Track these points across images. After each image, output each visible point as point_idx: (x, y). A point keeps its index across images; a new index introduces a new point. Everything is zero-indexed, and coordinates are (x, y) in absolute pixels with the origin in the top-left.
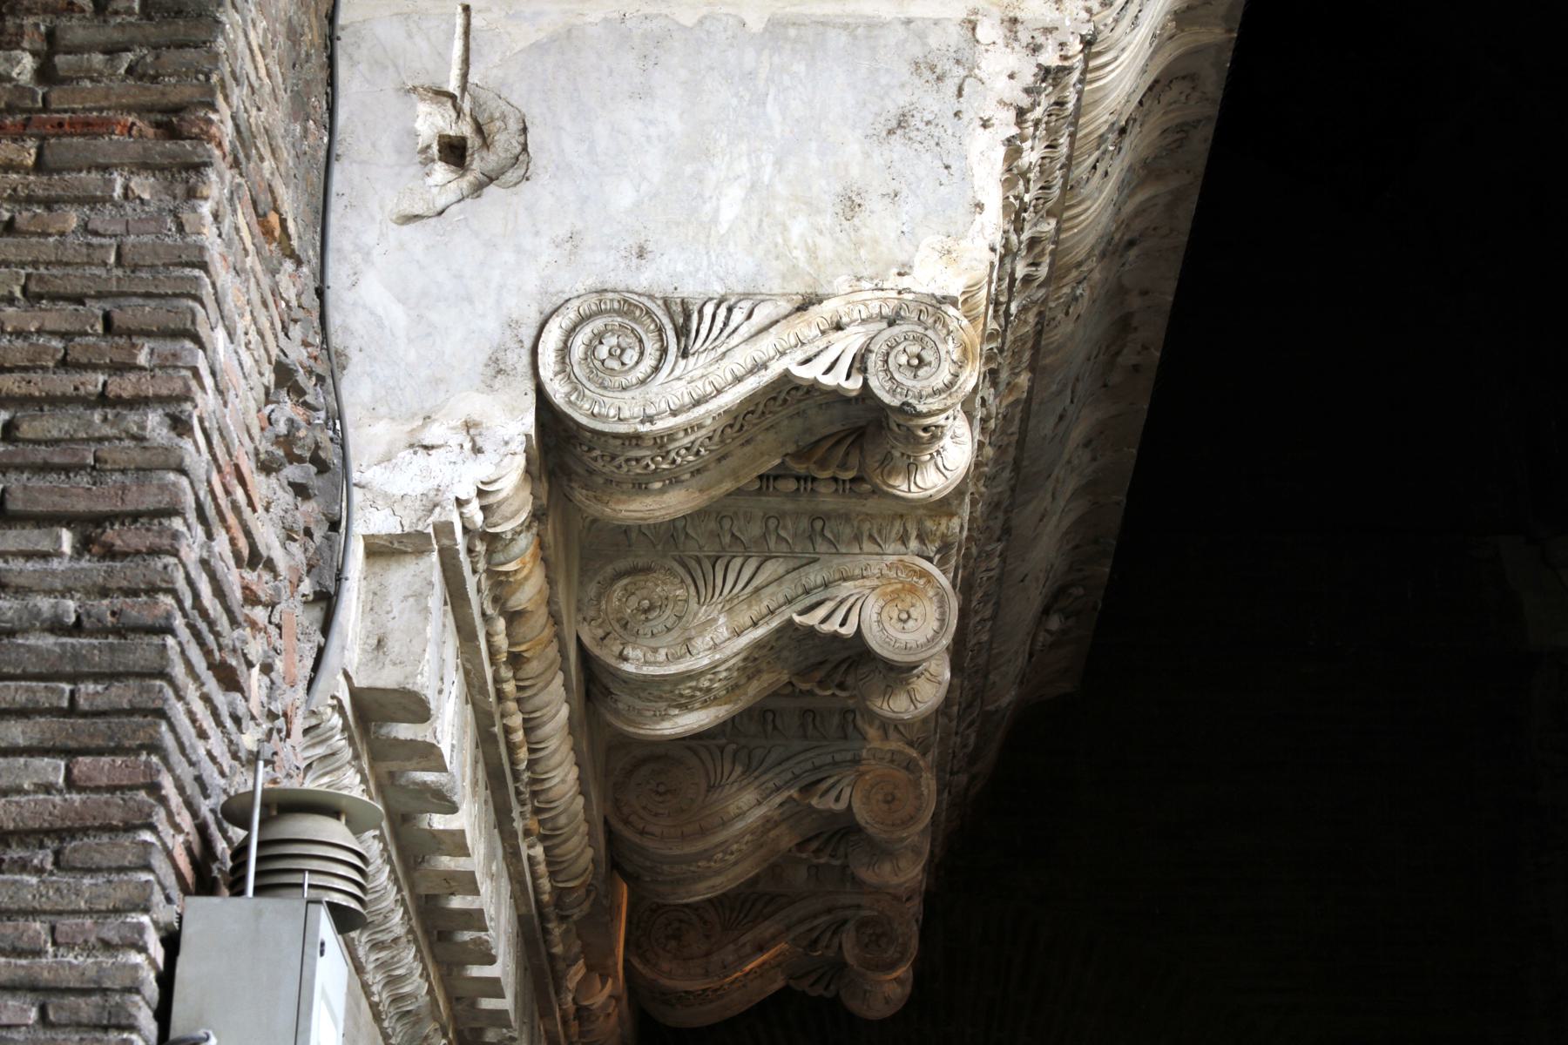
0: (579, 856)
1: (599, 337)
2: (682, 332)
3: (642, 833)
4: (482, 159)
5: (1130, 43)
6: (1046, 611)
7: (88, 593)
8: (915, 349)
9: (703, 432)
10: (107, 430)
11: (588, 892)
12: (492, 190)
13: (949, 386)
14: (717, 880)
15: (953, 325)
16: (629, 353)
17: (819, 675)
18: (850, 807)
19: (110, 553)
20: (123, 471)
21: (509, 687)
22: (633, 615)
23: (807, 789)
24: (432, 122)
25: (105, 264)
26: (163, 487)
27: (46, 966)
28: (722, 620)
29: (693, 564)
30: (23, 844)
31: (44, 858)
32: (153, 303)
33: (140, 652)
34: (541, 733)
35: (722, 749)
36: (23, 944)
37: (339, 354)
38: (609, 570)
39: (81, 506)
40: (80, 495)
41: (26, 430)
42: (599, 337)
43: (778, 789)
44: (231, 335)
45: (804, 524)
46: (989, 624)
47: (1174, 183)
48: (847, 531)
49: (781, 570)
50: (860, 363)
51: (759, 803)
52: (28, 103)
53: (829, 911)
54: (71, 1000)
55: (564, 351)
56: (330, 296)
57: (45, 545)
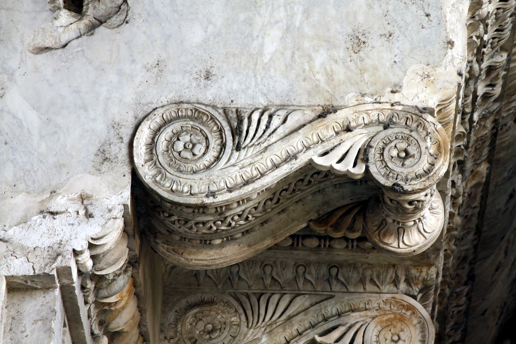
1: (177, 136)
2: (236, 132)
4: (95, 8)
8: (403, 145)
9: (251, 203)
12: (101, 30)
13: (427, 172)
16: (198, 147)
22: (201, 336)
29: (244, 299)
38: (184, 303)
42: (177, 136)
45: (324, 270)
48: (355, 276)
49: (307, 304)
50: (363, 155)
55: (152, 145)
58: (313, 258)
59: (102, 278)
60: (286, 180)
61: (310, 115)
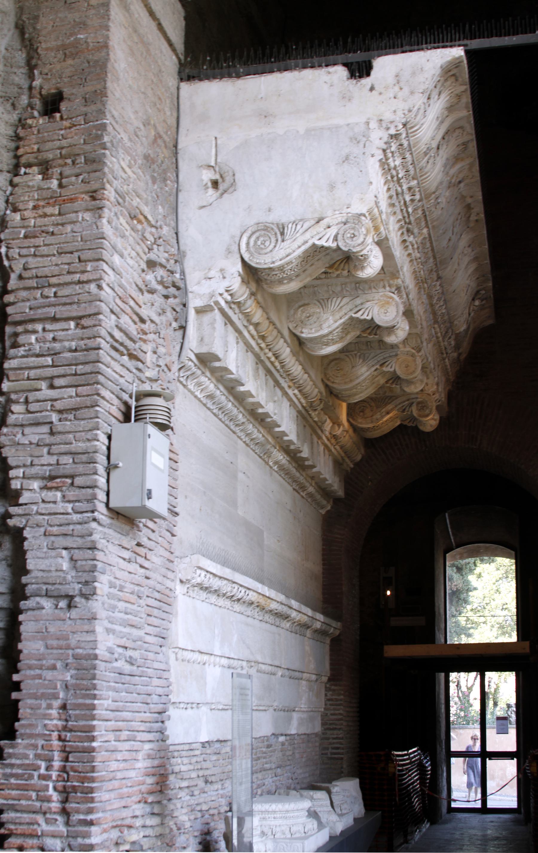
0: (312, 391)
1: (258, 238)
2: (282, 234)
3: (333, 383)
5: (425, 122)
6: (473, 299)
7: (78, 339)
8: (352, 232)
9: (294, 264)
10: (81, 291)
11: (321, 402)
12: (225, 195)
13: (363, 242)
14: (361, 395)
15: (364, 223)
17: (369, 331)
18: (395, 370)
19: (84, 328)
20: (85, 303)
21: (263, 345)
23: (382, 365)
24: (207, 176)
25: (77, 241)
26: (96, 307)
27: (73, 447)
28: (331, 318)
29: (321, 301)
30: (67, 413)
31: (71, 416)
32: (91, 251)
33: (92, 355)
34: (282, 357)
35: (356, 355)
36: (67, 441)
37: (184, 252)
38: (297, 306)
39: (75, 314)
40: (74, 311)
41: (59, 294)
42: (258, 238)
43: (373, 366)
44: (122, 256)
45: (353, 285)
46: (444, 307)
47: (468, 161)
48: (367, 286)
49: (348, 300)
50: (336, 239)
51: (368, 371)
52: (55, 195)
53: (408, 400)
54: (80, 456)
55: (248, 244)
56: (180, 235)
57: (66, 327)
58: (347, 280)
59: (239, 303)
60: (306, 251)
61: (313, 222)
